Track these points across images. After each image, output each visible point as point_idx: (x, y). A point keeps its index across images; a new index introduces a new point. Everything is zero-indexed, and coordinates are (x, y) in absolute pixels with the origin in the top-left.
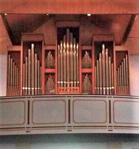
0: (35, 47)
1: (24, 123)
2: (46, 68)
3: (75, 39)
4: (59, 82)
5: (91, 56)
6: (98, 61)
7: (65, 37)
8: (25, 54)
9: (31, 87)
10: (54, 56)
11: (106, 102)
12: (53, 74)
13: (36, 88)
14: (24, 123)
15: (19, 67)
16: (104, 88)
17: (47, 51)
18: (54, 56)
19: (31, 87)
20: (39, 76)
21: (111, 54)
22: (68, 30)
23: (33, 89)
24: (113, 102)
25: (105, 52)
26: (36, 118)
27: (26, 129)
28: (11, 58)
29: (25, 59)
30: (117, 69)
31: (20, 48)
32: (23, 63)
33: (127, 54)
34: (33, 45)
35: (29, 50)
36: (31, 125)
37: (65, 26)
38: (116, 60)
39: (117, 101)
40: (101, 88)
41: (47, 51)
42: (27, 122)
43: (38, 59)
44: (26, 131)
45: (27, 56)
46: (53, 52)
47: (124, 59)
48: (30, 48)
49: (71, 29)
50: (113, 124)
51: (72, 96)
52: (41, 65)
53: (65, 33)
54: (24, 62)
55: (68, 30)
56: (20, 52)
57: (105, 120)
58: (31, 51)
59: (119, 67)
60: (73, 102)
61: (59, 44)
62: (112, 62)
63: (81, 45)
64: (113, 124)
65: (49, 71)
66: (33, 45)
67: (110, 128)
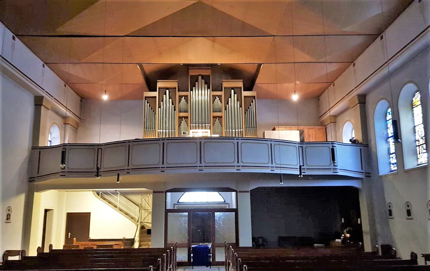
0: (169, 92)
1: (159, 163)
2: (180, 112)
3: (206, 85)
4: (242, 130)
5: (221, 101)
6: (227, 105)
7: (197, 83)
8: (161, 100)
9: (166, 129)
10: (187, 101)
11: (268, 145)
12: (186, 118)
13: (170, 131)
14: (197, 162)
15: (154, 111)
16: (234, 130)
17: (180, 97)
18: (187, 101)
19: (166, 129)
20: (173, 118)
21: (239, 99)
22: (200, 77)
23: (167, 131)
24: (241, 144)
25: (234, 97)
26: (246, 159)
27: (236, 167)
28: (147, 103)
29: (161, 103)
30: (245, 113)
31: (155, 94)
32: (159, 108)
33: (255, 99)
34: (167, 91)
35: (164, 96)
36: (203, 164)
37: (197, 74)
38: (19, 78)
39: (244, 142)
40: (231, 130)
41: (180, 97)
42: (199, 162)
43: (173, 104)
44: (270, 170)
45: (163, 101)
46: (186, 97)
47: (252, 103)
48: (165, 94)
49: (203, 77)
50: (274, 165)
51: (273, 140)
52: (175, 110)
53: (197, 81)
54: (160, 107)
55: (200, 77)
56: (155, 97)
57: (169, 163)
58: (166, 97)
59: (247, 111)
60: (306, 148)
61: (192, 90)
62: (241, 106)
63: (212, 91)
64: (203, 164)
65: (182, 114)
66: (167, 91)
67: (238, 168)
